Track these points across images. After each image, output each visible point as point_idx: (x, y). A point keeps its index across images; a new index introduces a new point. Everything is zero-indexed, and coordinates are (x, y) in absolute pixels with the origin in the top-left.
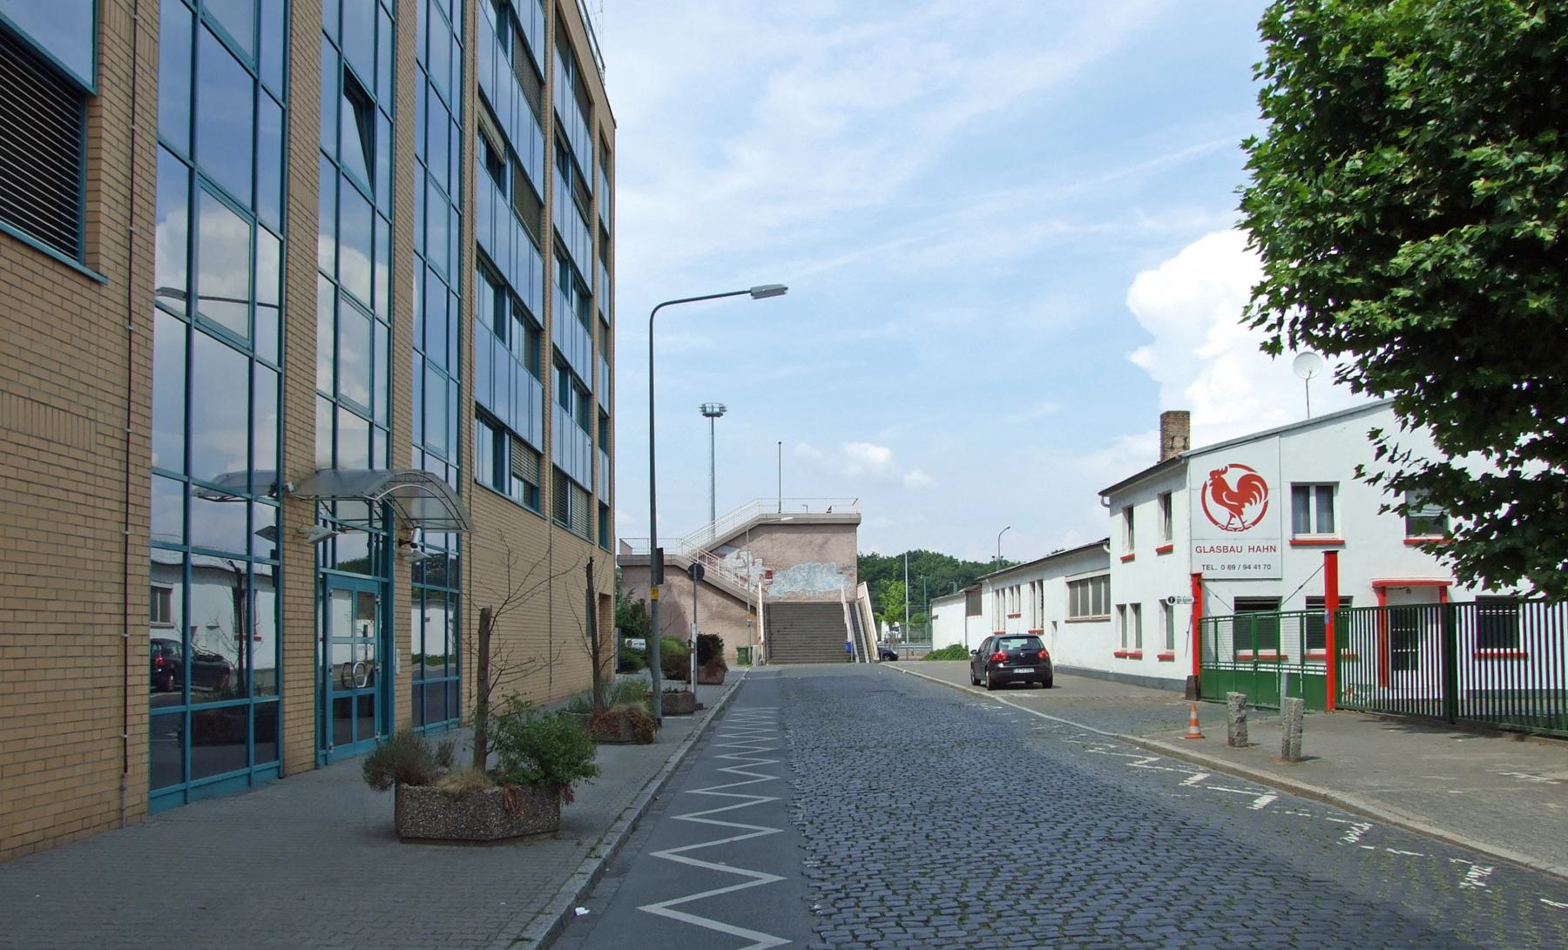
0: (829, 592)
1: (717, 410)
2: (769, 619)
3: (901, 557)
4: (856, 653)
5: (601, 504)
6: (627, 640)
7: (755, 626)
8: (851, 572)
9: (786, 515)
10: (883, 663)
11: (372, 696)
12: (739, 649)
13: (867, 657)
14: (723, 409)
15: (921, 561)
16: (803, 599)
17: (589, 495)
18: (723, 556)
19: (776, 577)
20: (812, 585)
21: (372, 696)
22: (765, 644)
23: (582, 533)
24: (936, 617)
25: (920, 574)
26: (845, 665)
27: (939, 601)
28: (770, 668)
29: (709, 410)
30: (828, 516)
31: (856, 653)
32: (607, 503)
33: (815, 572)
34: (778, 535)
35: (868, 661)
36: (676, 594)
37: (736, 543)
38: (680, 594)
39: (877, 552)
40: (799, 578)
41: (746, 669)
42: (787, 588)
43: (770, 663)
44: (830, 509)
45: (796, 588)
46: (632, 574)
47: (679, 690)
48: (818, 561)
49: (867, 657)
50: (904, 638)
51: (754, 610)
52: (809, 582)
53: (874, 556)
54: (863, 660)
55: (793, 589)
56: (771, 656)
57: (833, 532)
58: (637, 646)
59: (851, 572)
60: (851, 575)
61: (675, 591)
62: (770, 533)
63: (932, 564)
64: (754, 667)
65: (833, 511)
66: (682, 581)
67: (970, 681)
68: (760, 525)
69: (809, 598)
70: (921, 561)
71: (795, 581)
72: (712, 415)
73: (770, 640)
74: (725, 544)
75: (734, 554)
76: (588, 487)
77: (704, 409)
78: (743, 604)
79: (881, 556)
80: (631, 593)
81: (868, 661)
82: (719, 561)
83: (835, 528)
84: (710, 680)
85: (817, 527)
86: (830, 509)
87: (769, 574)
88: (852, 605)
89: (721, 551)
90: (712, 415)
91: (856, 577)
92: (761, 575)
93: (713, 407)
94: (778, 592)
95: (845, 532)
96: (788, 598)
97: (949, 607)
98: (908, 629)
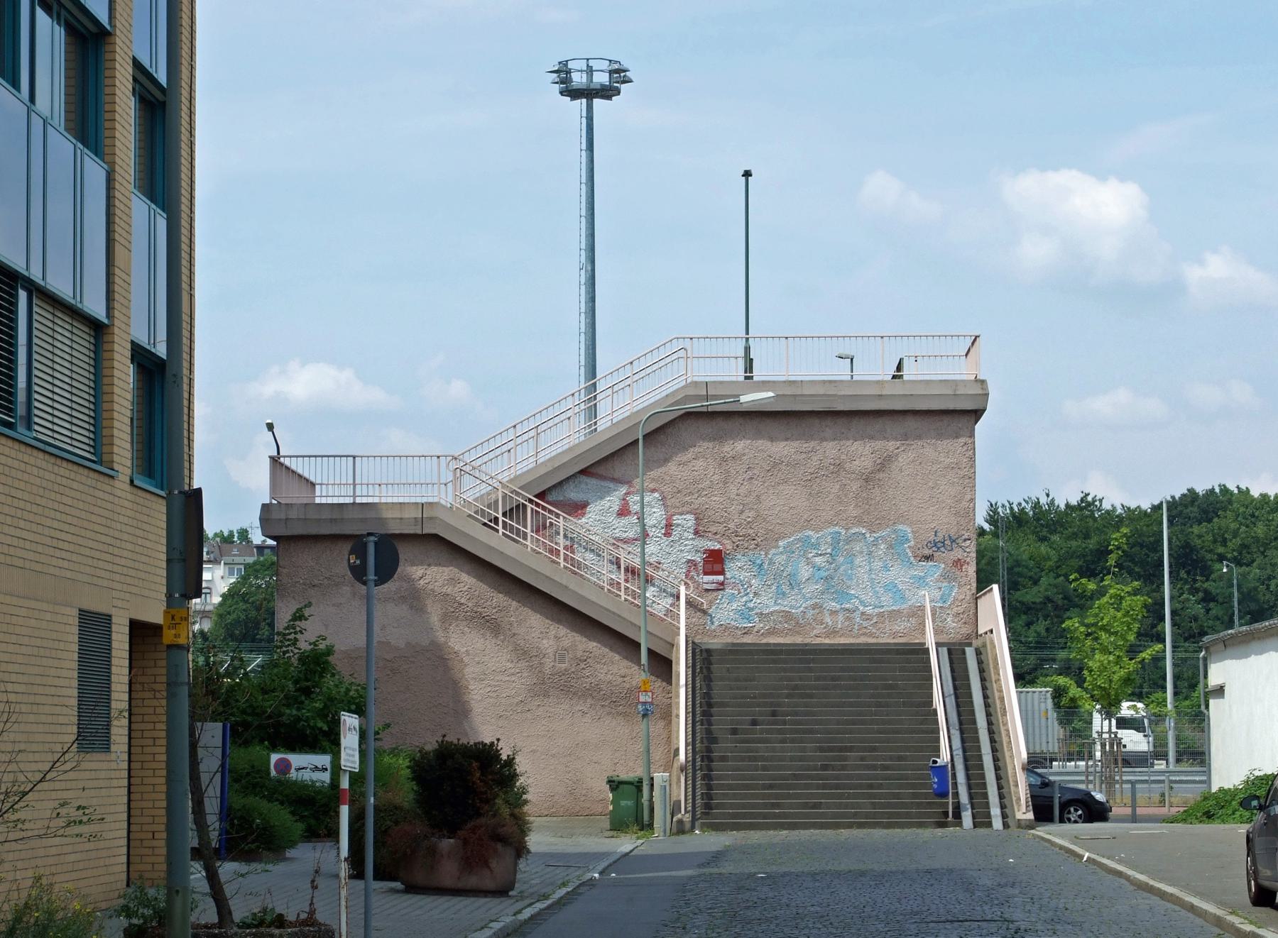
0: (894, 615)
1: (601, 78)
2: (707, 695)
3: (1157, 508)
4: (964, 798)
5: (140, 355)
6: (275, 757)
7: (668, 715)
8: (957, 554)
9: (765, 385)
10: (1042, 831)
11: (665, 786)
12: (615, 785)
13: (995, 811)
14: (619, 75)
15: (1227, 521)
16: (815, 637)
17: (98, 330)
18: (577, 508)
19: (736, 569)
20: (842, 595)
21: (665, 786)
22: (690, 769)
23: (76, 439)
24: (1220, 691)
25: (1221, 558)
26: (928, 834)
27: (1226, 643)
28: (704, 841)
29: (578, 79)
30: (897, 388)
31: (964, 798)
32: (161, 350)
33: (851, 556)
34: (740, 445)
35: (997, 823)
36: (435, 619)
37: (618, 469)
38: (446, 618)
39: (1095, 491)
40: (805, 572)
41: (626, 844)
42: (767, 603)
43: (704, 827)
44: (899, 368)
45: (796, 604)
46: (306, 561)
47: (291, 917)
48: (859, 521)
49: (995, 811)
50: (1159, 753)
51: (662, 665)
52: (832, 584)
53: (1086, 506)
54: (982, 820)
55: (785, 605)
56: (708, 806)
57: (905, 437)
58: (307, 776)
59: (957, 554)
60: (958, 563)
61: (434, 614)
62: (719, 438)
63: (1260, 530)
64: (658, 841)
65: (909, 373)
66: (453, 581)
67: (1241, 889)
68: (689, 415)
69: (833, 632)
70: (1227, 521)
71: (793, 583)
72: (589, 94)
73: (708, 758)
74: (584, 472)
75: (612, 501)
76: (95, 306)
77: (563, 73)
78: (627, 645)
79: (1106, 506)
80: (299, 616)
81: (997, 823)
82: (562, 522)
83: (911, 423)
84: (473, 881)
85: (857, 424)
86: (899, 368)
87: (715, 561)
88: (955, 654)
89: (573, 494)
90: (589, 94)
91: (971, 569)
92: (691, 563)
93: (590, 71)
94: (745, 613)
95: (940, 436)
96: (771, 632)
97: (1253, 659)
98: (1170, 723)
